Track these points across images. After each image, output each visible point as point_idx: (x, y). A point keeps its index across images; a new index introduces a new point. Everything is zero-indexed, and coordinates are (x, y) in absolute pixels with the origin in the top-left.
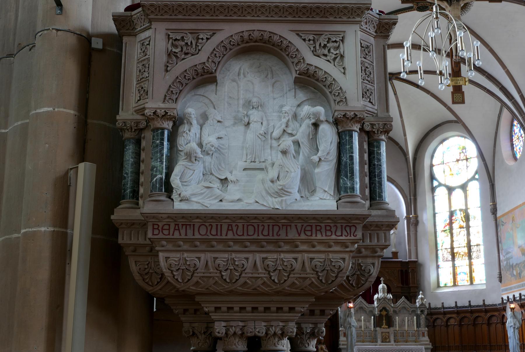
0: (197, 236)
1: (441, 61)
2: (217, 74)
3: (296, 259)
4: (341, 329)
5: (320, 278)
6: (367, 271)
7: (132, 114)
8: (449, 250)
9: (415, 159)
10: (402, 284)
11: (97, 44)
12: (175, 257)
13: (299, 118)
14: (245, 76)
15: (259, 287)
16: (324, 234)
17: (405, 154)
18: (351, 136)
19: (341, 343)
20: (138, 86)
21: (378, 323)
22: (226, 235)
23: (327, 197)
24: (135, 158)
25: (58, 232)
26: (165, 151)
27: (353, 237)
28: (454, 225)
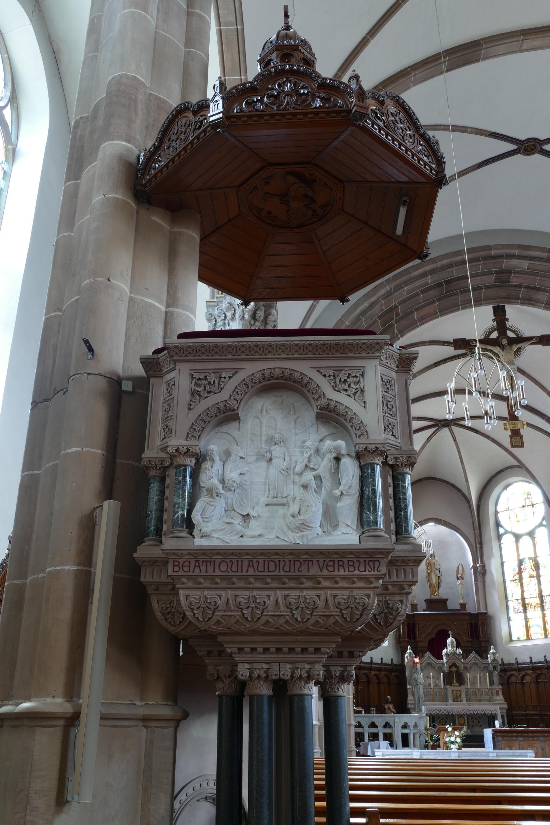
0: (218, 573)
1: (486, 402)
2: (240, 412)
3: (319, 596)
4: (408, 687)
5: (345, 616)
6: (395, 609)
7: (158, 452)
8: (520, 601)
9: (479, 506)
10: (472, 637)
11: (127, 386)
12: (195, 594)
13: (321, 453)
14: (267, 413)
15: (281, 626)
16: (347, 569)
17: (468, 500)
18: (373, 470)
19: (409, 702)
20: (163, 425)
21: (448, 681)
22: (247, 572)
23: (349, 531)
24: (159, 495)
25: (81, 570)
26: (187, 487)
27: (376, 573)
28: (523, 574)
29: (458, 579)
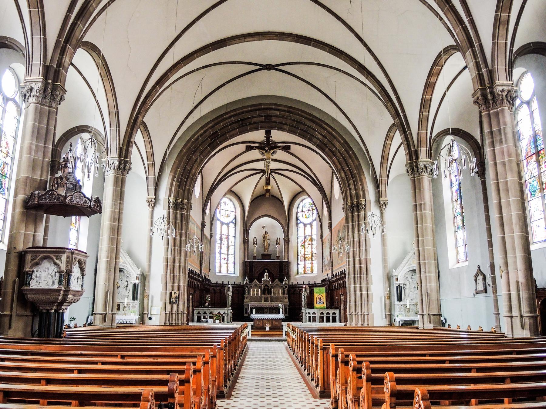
21: (263, 292)
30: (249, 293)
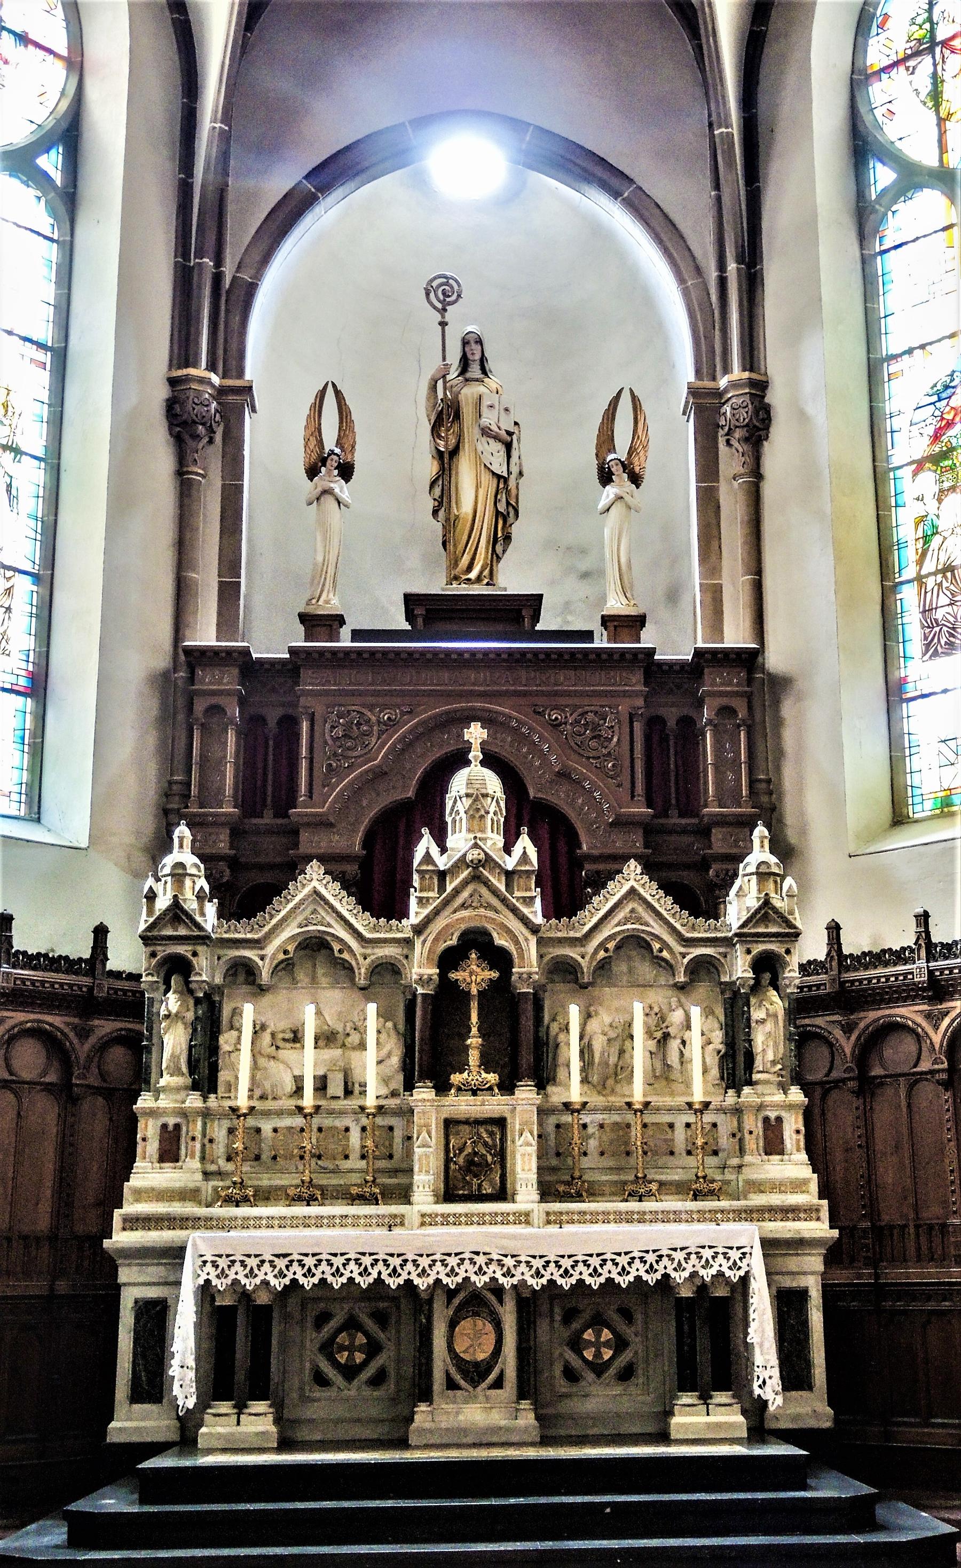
17: (915, 1066)
21: (429, 1058)
29: (606, 477)
30: (205, 1071)
